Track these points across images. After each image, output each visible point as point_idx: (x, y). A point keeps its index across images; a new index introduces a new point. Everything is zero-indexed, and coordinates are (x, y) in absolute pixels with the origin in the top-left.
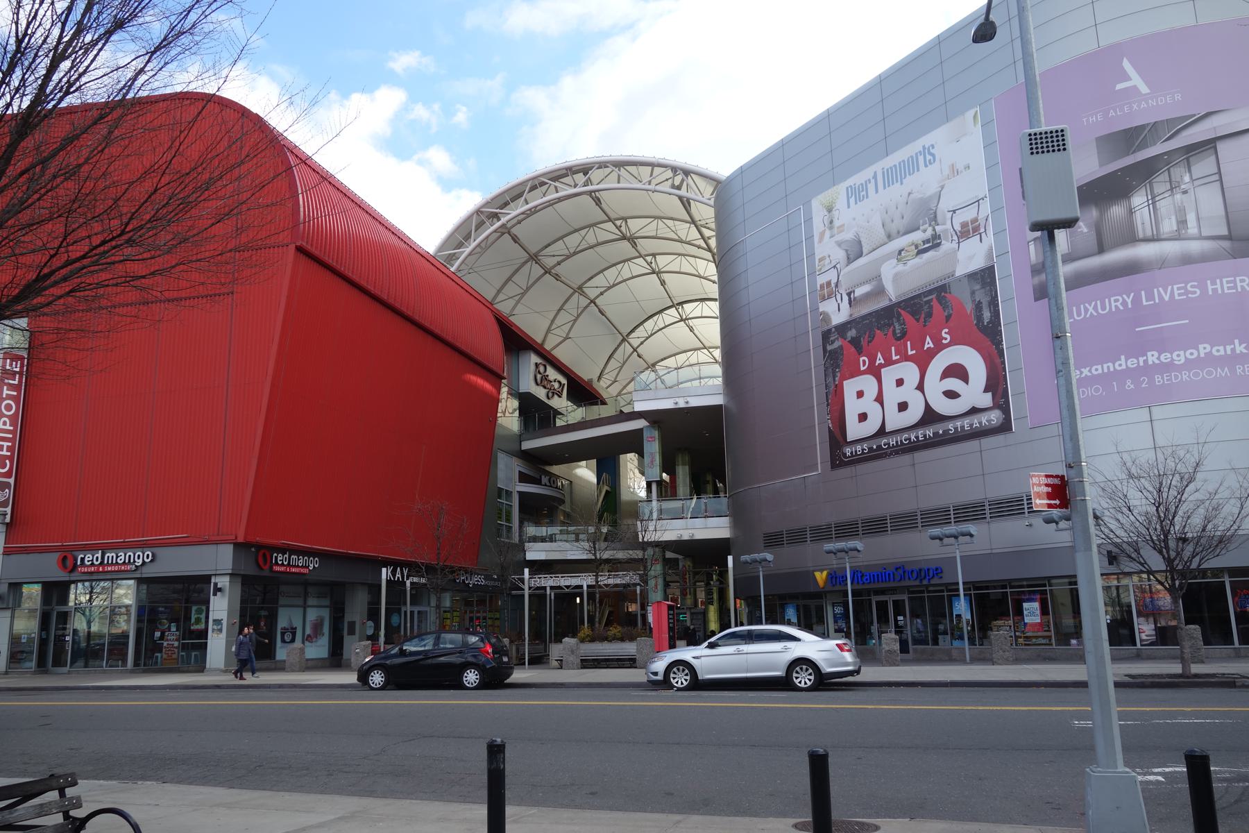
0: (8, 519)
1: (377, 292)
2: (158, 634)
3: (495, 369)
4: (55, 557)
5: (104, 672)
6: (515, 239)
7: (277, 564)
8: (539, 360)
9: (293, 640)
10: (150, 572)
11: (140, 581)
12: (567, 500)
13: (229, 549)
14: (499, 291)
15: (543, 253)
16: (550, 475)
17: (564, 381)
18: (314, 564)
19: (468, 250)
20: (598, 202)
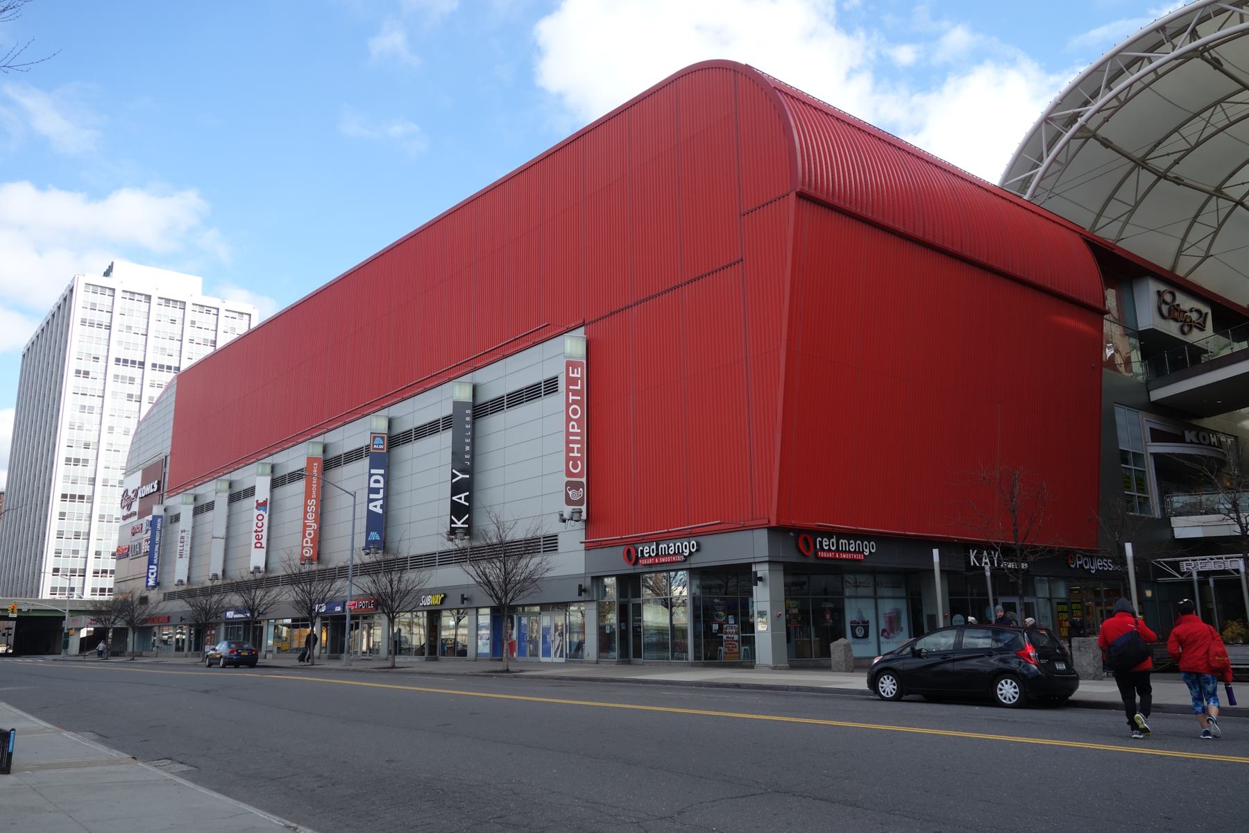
0: (584, 516)
1: (909, 230)
2: (715, 627)
3: (1091, 302)
4: (621, 551)
5: (670, 664)
6: (1106, 143)
7: (822, 549)
8: (1162, 288)
9: (866, 635)
10: (700, 561)
11: (693, 572)
12: (1231, 458)
13: (763, 534)
14: (1099, 215)
15: (1227, 184)
16: (1200, 429)
17: (1206, 309)
18: (869, 549)
19: (1041, 170)
20: (1216, 64)
